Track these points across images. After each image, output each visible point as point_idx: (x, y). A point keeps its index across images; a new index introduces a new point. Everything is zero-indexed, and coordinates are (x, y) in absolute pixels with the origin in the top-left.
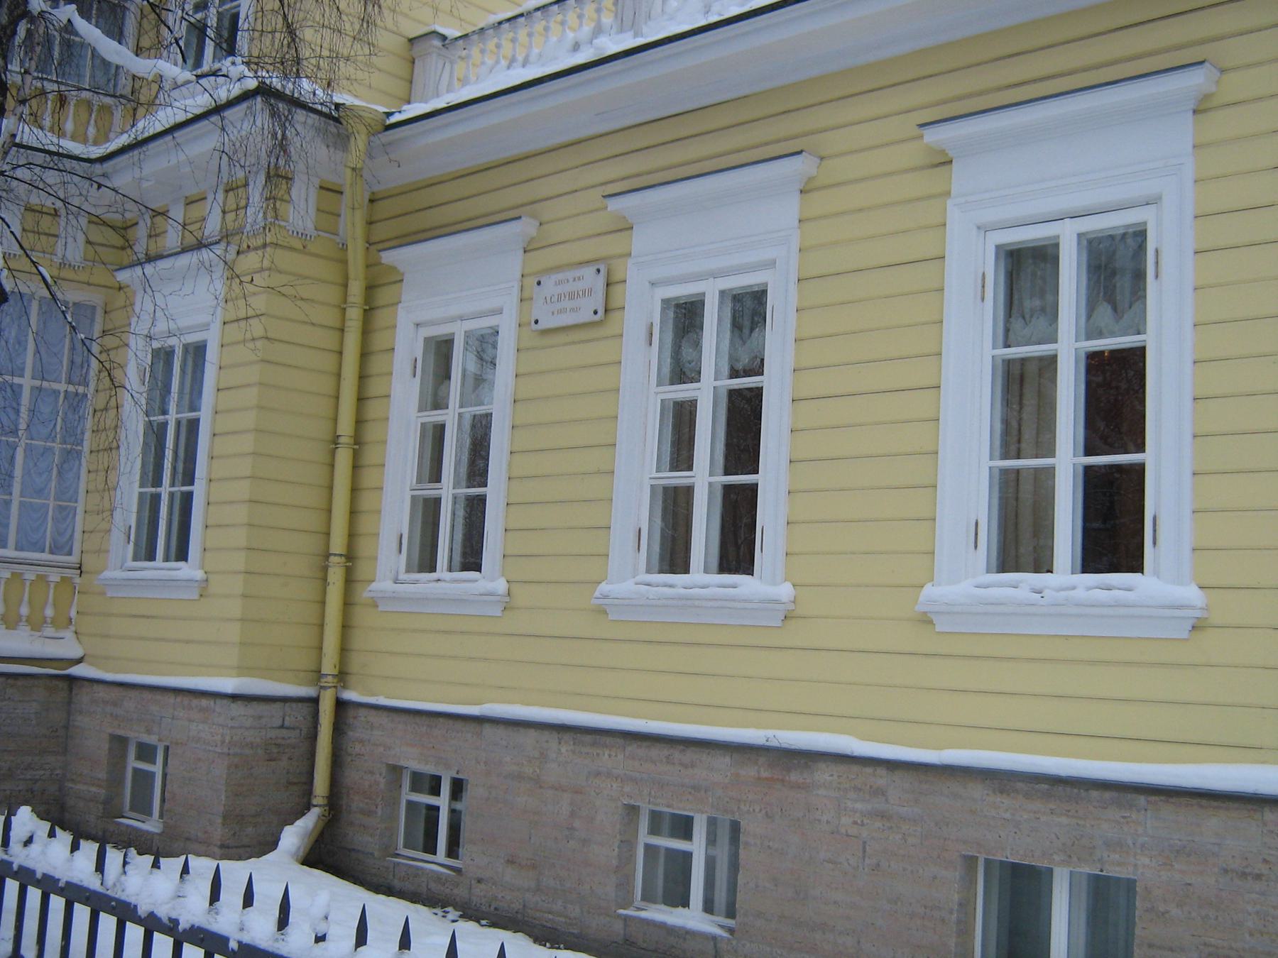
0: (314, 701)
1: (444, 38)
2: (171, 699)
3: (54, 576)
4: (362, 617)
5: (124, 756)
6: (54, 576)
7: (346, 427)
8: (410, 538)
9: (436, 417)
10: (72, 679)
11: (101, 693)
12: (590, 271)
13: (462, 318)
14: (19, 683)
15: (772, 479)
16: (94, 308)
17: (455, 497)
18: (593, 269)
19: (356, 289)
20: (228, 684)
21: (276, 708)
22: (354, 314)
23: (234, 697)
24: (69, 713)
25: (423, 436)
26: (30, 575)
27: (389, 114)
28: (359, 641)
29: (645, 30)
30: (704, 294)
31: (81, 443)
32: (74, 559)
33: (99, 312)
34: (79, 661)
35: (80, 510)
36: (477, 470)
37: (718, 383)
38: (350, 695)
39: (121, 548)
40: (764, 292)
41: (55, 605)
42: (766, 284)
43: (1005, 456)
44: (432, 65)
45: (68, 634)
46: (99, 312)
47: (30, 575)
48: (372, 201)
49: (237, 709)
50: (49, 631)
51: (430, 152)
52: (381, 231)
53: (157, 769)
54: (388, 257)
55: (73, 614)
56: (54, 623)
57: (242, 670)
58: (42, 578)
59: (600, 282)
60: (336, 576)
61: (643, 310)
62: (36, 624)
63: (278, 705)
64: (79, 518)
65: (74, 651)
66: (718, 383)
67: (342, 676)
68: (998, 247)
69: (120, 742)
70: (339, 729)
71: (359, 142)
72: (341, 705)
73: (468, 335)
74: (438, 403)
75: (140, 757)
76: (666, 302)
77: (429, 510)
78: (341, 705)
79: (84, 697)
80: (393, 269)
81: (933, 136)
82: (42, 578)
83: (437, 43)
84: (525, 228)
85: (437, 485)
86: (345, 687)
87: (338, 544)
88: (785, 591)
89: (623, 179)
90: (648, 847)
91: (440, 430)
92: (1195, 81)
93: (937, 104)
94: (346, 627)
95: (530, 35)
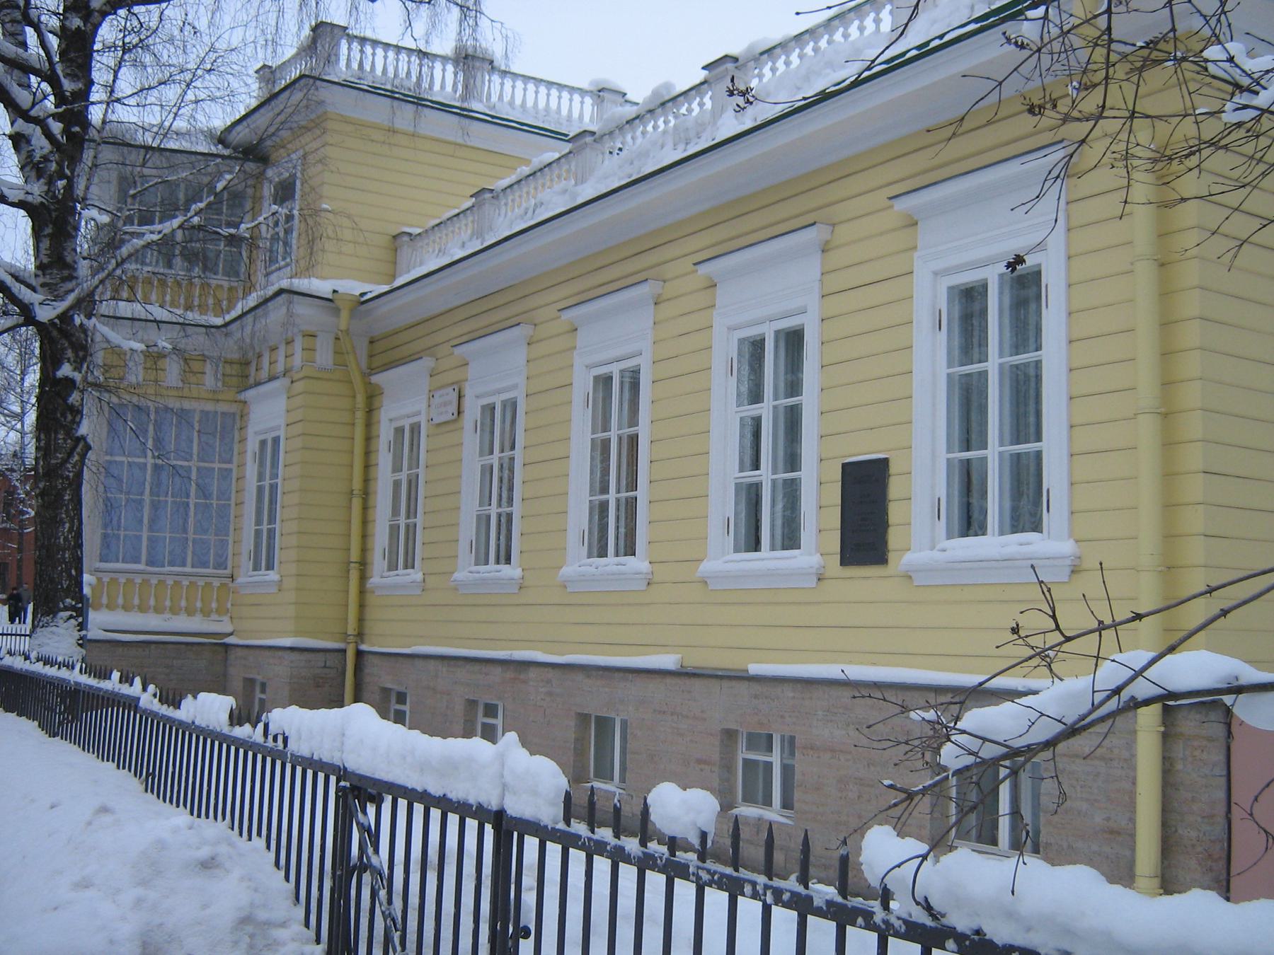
0: (344, 651)
1: (410, 234)
2: (267, 653)
3: (216, 583)
4: (371, 600)
5: (253, 691)
6: (216, 583)
7: (357, 485)
8: (948, 502)
9: (754, 410)
10: (226, 646)
11: (240, 652)
12: (450, 389)
13: (499, 392)
14: (194, 648)
15: (1054, 447)
16: (234, 414)
17: (774, 482)
18: (450, 389)
19: (360, 399)
20: (287, 642)
21: (320, 656)
22: (360, 415)
23: (292, 649)
24: (226, 666)
25: (742, 426)
26: (201, 582)
27: (362, 295)
28: (372, 614)
29: (487, 237)
30: (1039, 265)
31: (229, 499)
32: (228, 572)
33: (238, 417)
34: (231, 634)
35: (231, 542)
36: (1026, 421)
37: (951, 370)
38: (364, 647)
39: (246, 563)
40: (1039, 273)
41: (187, 600)
42: (1039, 265)
43: (1017, 440)
44: (405, 253)
45: (226, 619)
46: (238, 417)
47: (201, 582)
48: (371, 342)
49: (294, 656)
50: (214, 616)
51: (392, 314)
52: (377, 361)
53: (776, 759)
54: (375, 379)
55: (229, 606)
56: (218, 612)
57: (297, 633)
58: (208, 584)
59: (455, 395)
60: (354, 575)
61: (583, 384)
62: (206, 613)
63: (322, 654)
64: (230, 546)
65: (229, 629)
66: (951, 370)
67: (360, 635)
68: (950, 289)
69: (472, 704)
70: (358, 669)
71: (345, 314)
72: (360, 654)
73: (777, 333)
74: (756, 396)
75: (486, 715)
76: (741, 341)
77: (752, 496)
78: (360, 654)
79: (233, 655)
80: (377, 385)
81: (901, 205)
82: (208, 584)
83: (406, 238)
84: (427, 363)
85: (757, 472)
86: (363, 642)
87: (355, 555)
88: (1067, 547)
89: (903, 180)
90: (746, 762)
91: (757, 421)
92: (644, 290)
93: (579, 293)
94: (362, 606)
95: (536, 189)
